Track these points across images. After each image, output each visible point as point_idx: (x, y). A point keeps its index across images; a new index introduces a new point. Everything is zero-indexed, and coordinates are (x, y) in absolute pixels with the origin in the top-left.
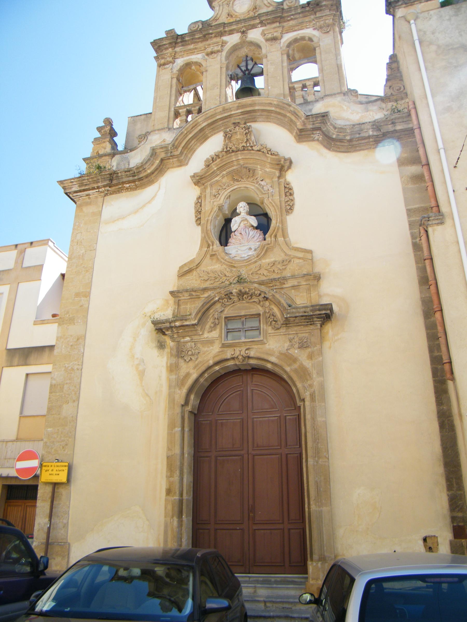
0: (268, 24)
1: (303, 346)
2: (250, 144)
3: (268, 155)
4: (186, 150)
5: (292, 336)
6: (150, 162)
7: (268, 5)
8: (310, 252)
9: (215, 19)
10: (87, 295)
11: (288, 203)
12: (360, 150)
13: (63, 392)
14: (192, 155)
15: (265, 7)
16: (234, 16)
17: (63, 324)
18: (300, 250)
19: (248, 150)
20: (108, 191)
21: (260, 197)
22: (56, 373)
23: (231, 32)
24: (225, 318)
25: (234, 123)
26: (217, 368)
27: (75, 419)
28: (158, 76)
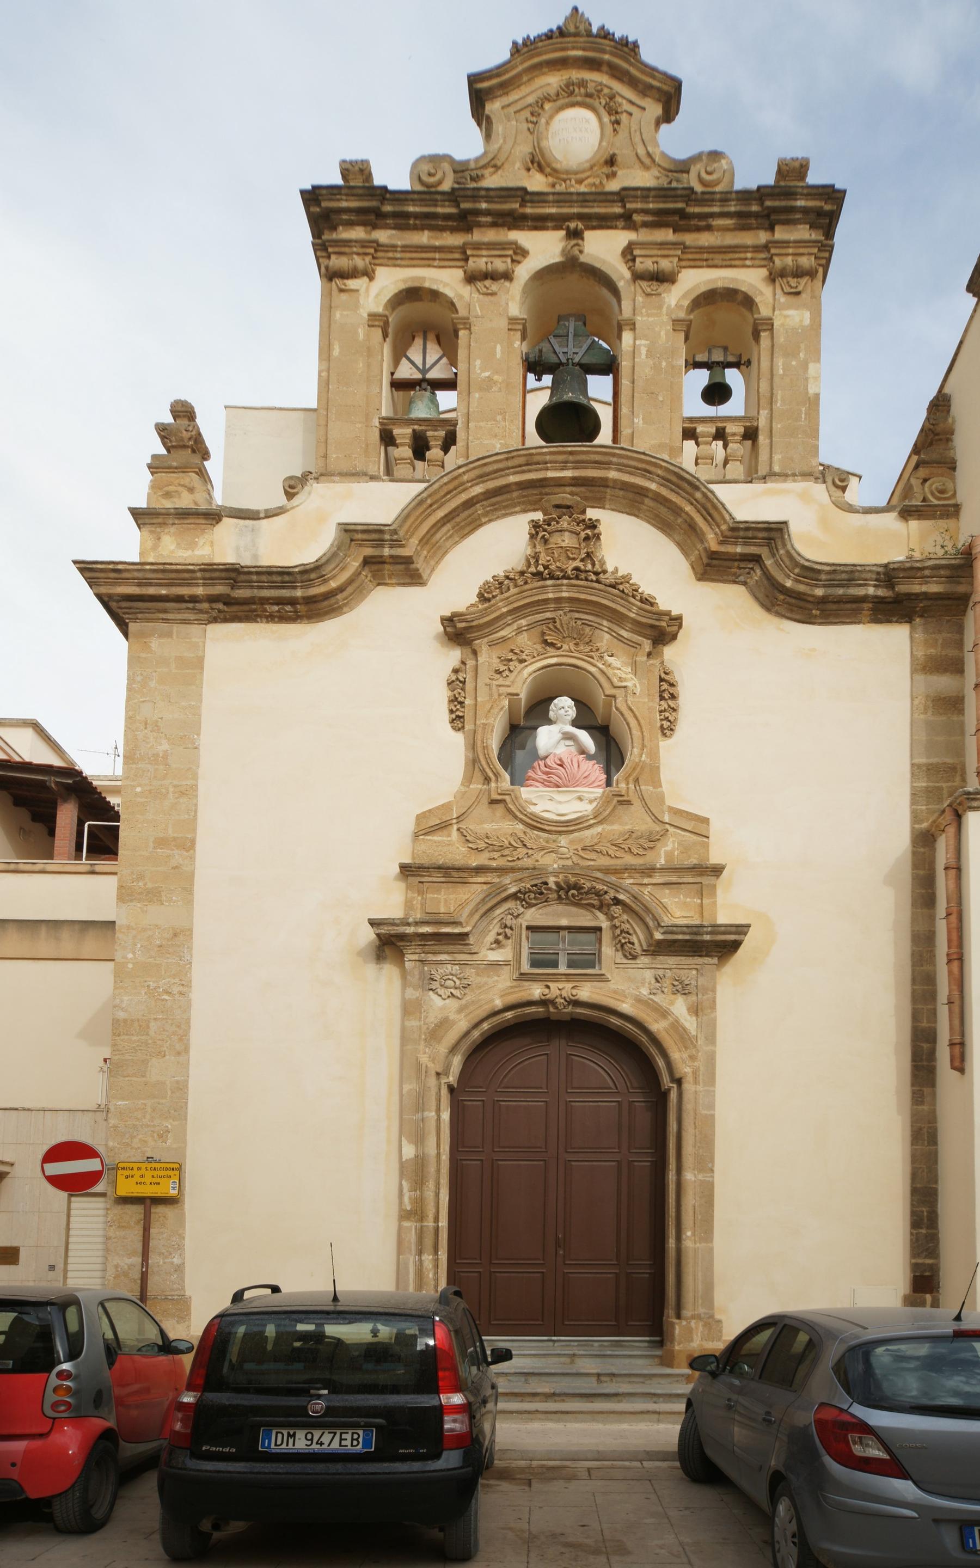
0: (645, 225)
1: (682, 989)
2: (593, 565)
3: (632, 600)
4: (428, 547)
5: (661, 972)
6: (337, 561)
7: (647, 161)
8: (706, 821)
9: (492, 163)
10: (189, 845)
11: (667, 714)
12: (835, 623)
13: (147, 1034)
14: (438, 563)
15: (637, 165)
16: (548, 170)
17: (131, 901)
18: (685, 815)
19: (586, 580)
20: (220, 611)
21: (608, 692)
22: (126, 998)
23: (539, 224)
24: (528, 928)
25: (557, 506)
26: (509, 1015)
27: (181, 1088)
28: (327, 309)
